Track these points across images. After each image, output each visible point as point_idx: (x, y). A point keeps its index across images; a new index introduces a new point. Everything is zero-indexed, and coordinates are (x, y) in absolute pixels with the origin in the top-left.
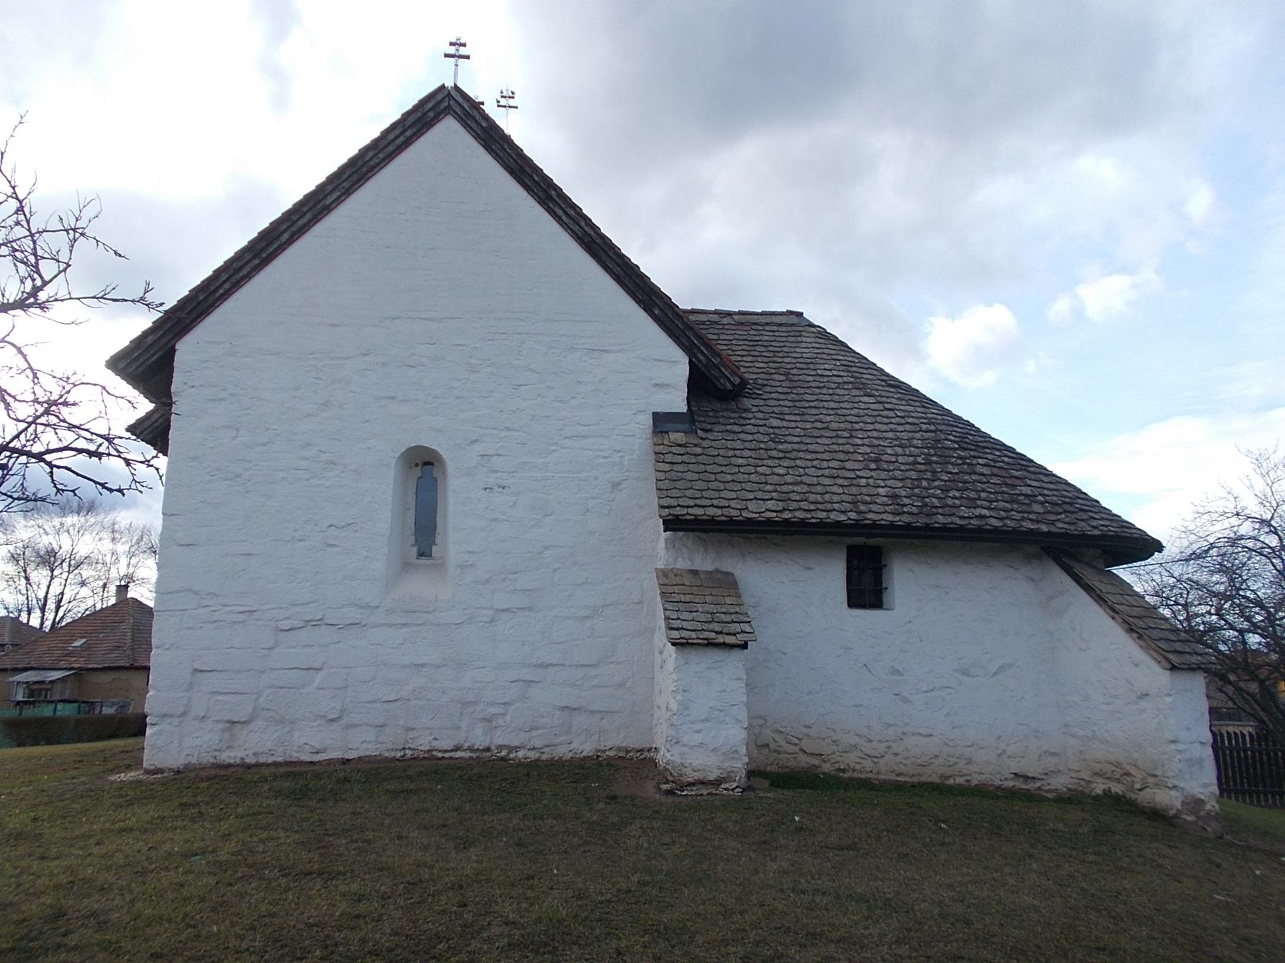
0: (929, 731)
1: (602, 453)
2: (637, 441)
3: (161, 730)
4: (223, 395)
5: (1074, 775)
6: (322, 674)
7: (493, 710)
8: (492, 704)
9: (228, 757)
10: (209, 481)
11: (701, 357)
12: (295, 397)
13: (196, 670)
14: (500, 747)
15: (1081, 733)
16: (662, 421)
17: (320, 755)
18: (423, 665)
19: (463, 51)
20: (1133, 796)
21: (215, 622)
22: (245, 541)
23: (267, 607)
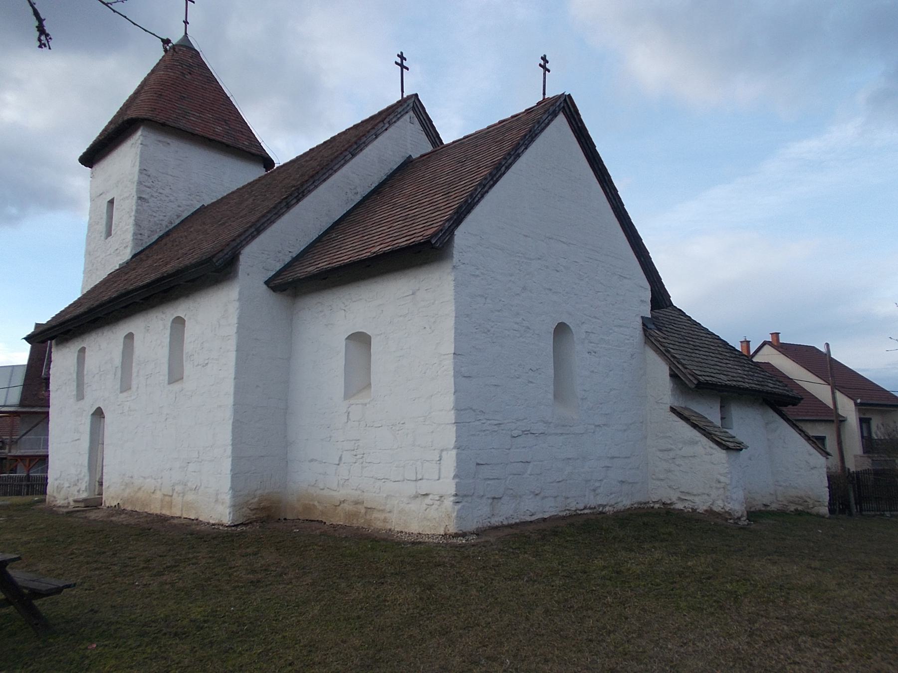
3: (463, 506)
5: (780, 503)
6: (531, 465)
9: (496, 521)
11: (657, 289)
12: (510, 280)
13: (478, 464)
14: (600, 505)
15: (784, 484)
17: (533, 517)
20: (809, 511)
21: (484, 431)
22: (494, 376)
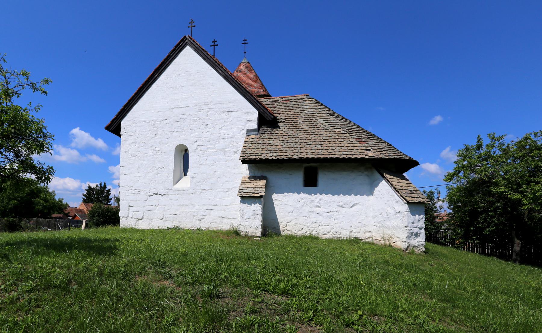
0: (327, 224)
1: (232, 143)
2: (242, 138)
4: (132, 134)
6: (158, 207)
7: (202, 217)
8: (201, 216)
10: (130, 157)
16: (249, 131)
18: (183, 205)
19: (246, 42)
23: (145, 190)
